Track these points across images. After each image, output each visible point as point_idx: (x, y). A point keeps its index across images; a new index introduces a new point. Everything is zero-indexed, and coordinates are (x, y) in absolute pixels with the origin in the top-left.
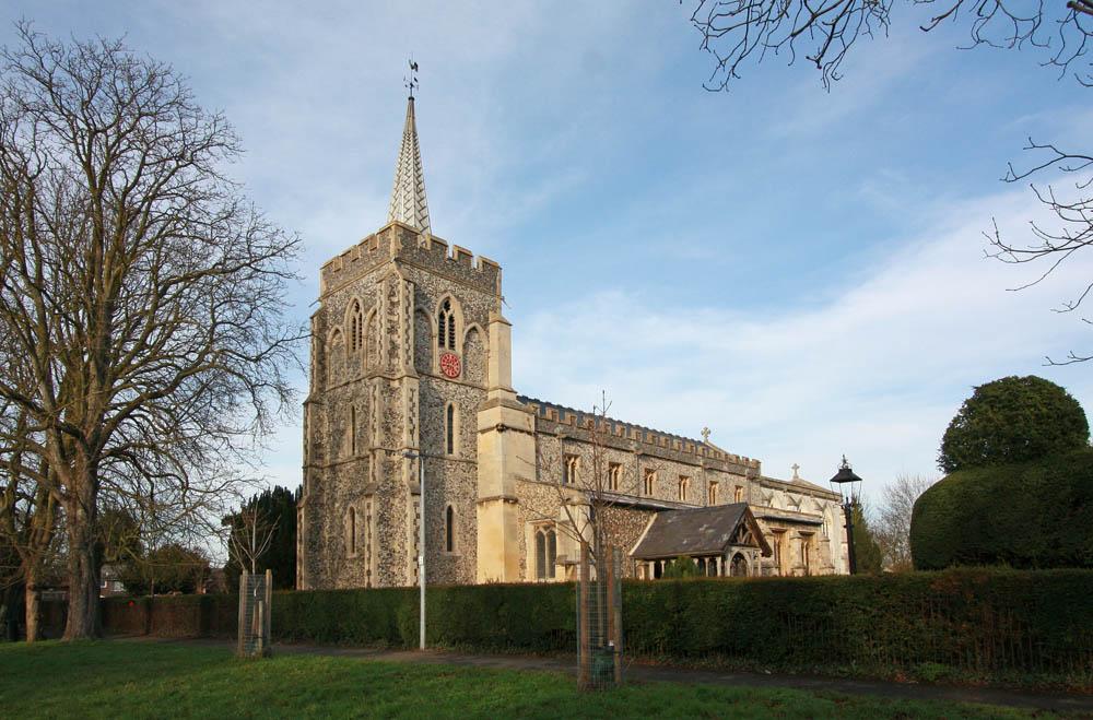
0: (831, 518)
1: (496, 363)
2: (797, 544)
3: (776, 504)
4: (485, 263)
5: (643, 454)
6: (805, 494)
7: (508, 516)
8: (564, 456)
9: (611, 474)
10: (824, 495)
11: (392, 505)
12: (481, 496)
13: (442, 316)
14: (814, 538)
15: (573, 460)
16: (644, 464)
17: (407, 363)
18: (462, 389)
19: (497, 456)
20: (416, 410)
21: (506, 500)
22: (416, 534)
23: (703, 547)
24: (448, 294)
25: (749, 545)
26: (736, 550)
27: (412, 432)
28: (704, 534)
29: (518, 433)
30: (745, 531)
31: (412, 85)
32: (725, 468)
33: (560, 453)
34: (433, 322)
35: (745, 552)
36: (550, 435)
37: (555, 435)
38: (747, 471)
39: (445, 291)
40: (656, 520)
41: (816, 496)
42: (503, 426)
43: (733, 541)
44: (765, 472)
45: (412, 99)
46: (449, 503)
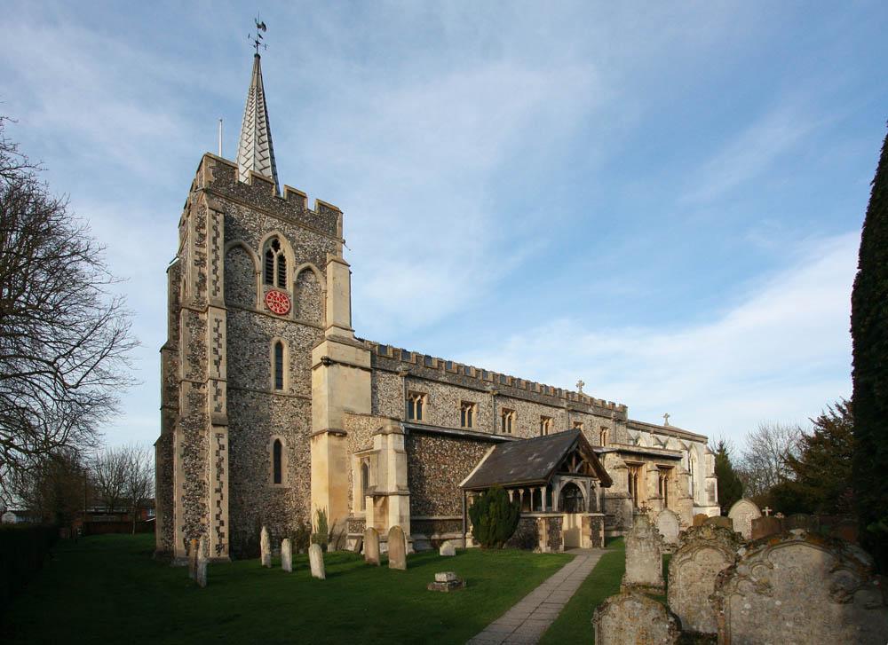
0: (696, 456)
1: (331, 301)
2: (654, 477)
3: (642, 443)
4: (322, 206)
5: (573, 410)
6: (671, 436)
7: (331, 448)
8: (462, 403)
9: (542, 426)
10: (690, 437)
11: (201, 437)
12: (314, 431)
13: (269, 255)
14: (673, 470)
15: (419, 397)
16: (501, 404)
17: (215, 295)
18: (293, 327)
19: (331, 391)
20: (223, 341)
21: (331, 433)
22: (218, 466)
23: (529, 476)
24: (275, 232)
25: (580, 474)
26: (566, 479)
27: (217, 363)
28: (531, 464)
29: (349, 369)
30: (579, 459)
31: (257, 43)
32: (590, 411)
33: (403, 391)
34: (256, 259)
35: (579, 482)
36: (391, 372)
37: (397, 373)
38: (613, 414)
39: (271, 229)
40: (493, 452)
41: (681, 438)
42: (328, 359)
43: (563, 468)
44: (631, 416)
45: (257, 56)
46: (275, 437)
